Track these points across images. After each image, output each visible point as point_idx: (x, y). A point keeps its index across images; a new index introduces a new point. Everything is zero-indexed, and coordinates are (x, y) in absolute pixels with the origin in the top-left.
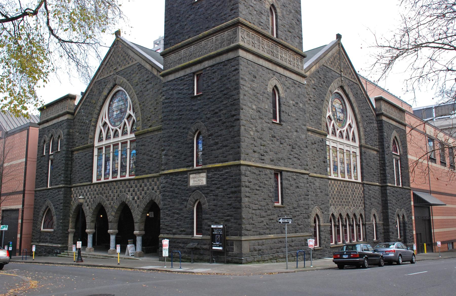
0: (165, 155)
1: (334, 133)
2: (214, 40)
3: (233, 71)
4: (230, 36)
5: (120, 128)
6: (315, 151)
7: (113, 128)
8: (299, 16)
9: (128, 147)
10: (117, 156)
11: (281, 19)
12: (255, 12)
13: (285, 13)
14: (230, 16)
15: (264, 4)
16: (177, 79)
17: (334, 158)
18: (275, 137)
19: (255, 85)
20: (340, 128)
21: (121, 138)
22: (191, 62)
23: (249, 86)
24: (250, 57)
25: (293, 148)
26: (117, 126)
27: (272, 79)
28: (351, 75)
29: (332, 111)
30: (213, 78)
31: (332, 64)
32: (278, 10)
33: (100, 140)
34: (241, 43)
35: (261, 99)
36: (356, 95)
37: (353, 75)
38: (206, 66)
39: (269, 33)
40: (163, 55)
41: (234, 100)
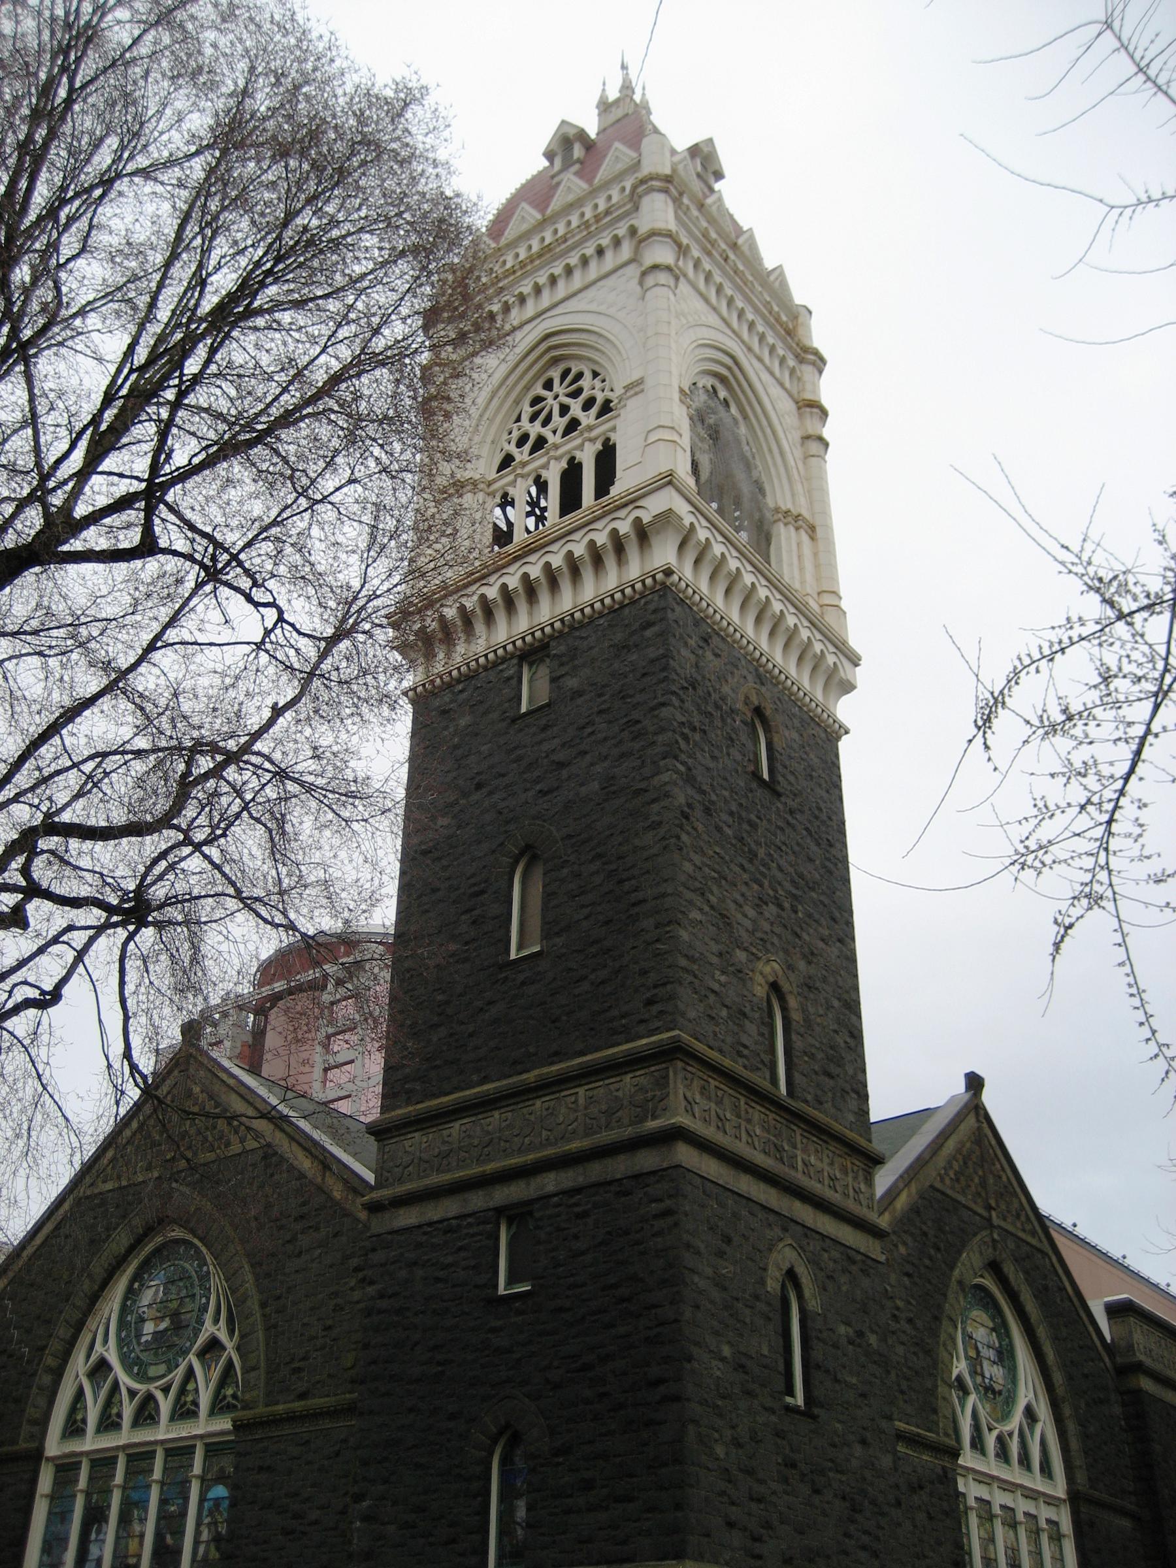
0: (367, 1518)
1: (978, 1444)
2: (581, 1101)
3: (656, 1217)
4: (642, 1089)
5: (166, 1390)
6: (921, 1516)
7: (136, 1386)
8: (854, 1018)
9: (197, 1469)
10: (143, 1505)
11: (802, 1030)
12: (724, 1013)
13: (811, 1010)
14: (642, 1021)
15: (749, 983)
16: (430, 1224)
17: (984, 1549)
18: (793, 1466)
19: (727, 1269)
20: (997, 1421)
21: (164, 1431)
22: (490, 1167)
23: (709, 1271)
24: (711, 1168)
25: (854, 1510)
26: (152, 1380)
27: (781, 1245)
28: (1023, 1218)
29: (967, 1357)
30: (576, 1237)
31: (958, 1180)
32: (792, 1002)
33: (74, 1428)
34: (683, 1120)
35: (748, 1320)
36: (1042, 1294)
37: (1028, 1219)
38: (551, 1188)
39: (760, 1080)
40: (378, 1131)
41: (662, 1324)
